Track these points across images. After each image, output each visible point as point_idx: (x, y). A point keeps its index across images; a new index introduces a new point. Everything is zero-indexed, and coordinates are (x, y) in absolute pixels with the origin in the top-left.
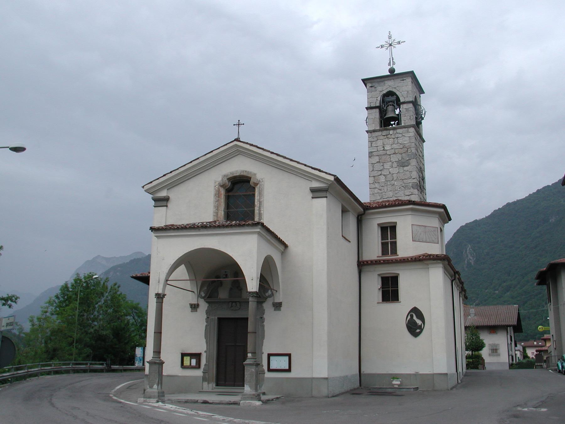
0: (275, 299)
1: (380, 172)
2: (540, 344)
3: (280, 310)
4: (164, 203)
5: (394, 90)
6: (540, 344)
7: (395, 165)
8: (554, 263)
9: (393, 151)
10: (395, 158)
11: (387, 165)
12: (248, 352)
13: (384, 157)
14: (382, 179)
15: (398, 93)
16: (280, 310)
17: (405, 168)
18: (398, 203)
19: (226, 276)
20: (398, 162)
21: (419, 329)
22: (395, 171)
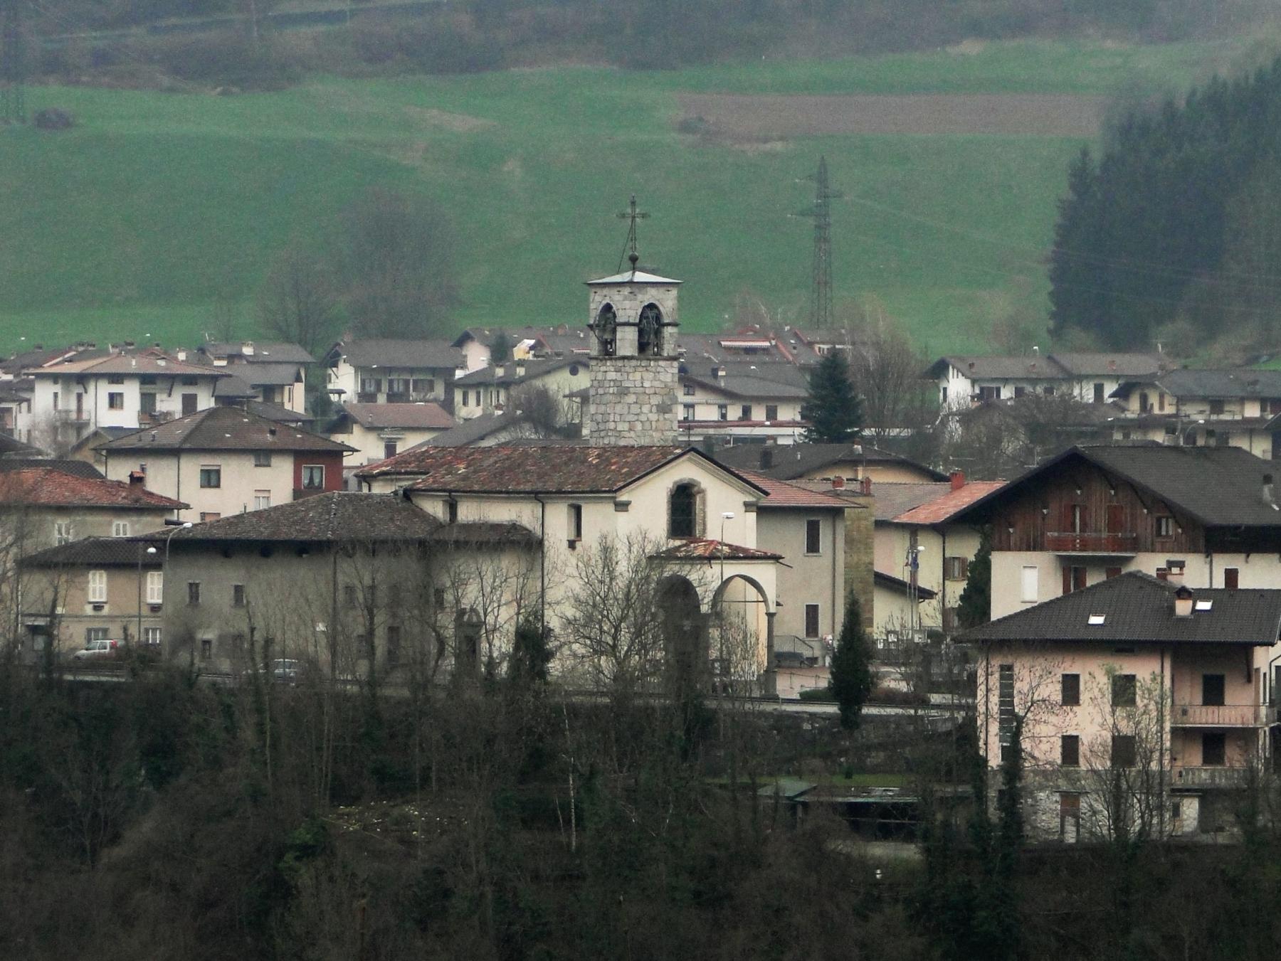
0: (255, 366)
1: (636, 417)
2: (1096, 620)
3: (627, 511)
4: (624, 508)
5: (657, 303)
6: (299, 436)
7: (654, 409)
8: (968, 507)
9: (652, 391)
10: (655, 400)
11: (646, 409)
12: (1207, 586)
13: (641, 397)
14: (639, 426)
15: (661, 308)
16: (627, 511)
17: (667, 416)
18: (533, 844)
19: (1065, 690)
20: (658, 406)
21: (1137, 577)
22: (653, 417)
